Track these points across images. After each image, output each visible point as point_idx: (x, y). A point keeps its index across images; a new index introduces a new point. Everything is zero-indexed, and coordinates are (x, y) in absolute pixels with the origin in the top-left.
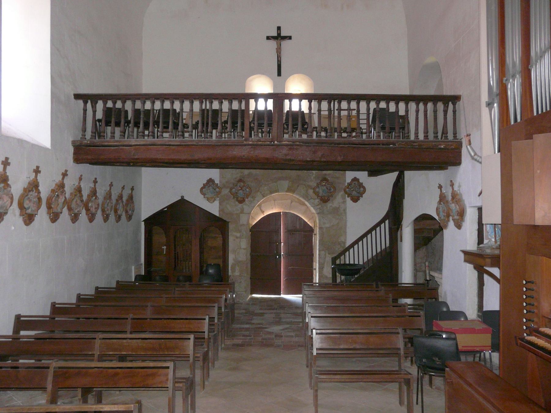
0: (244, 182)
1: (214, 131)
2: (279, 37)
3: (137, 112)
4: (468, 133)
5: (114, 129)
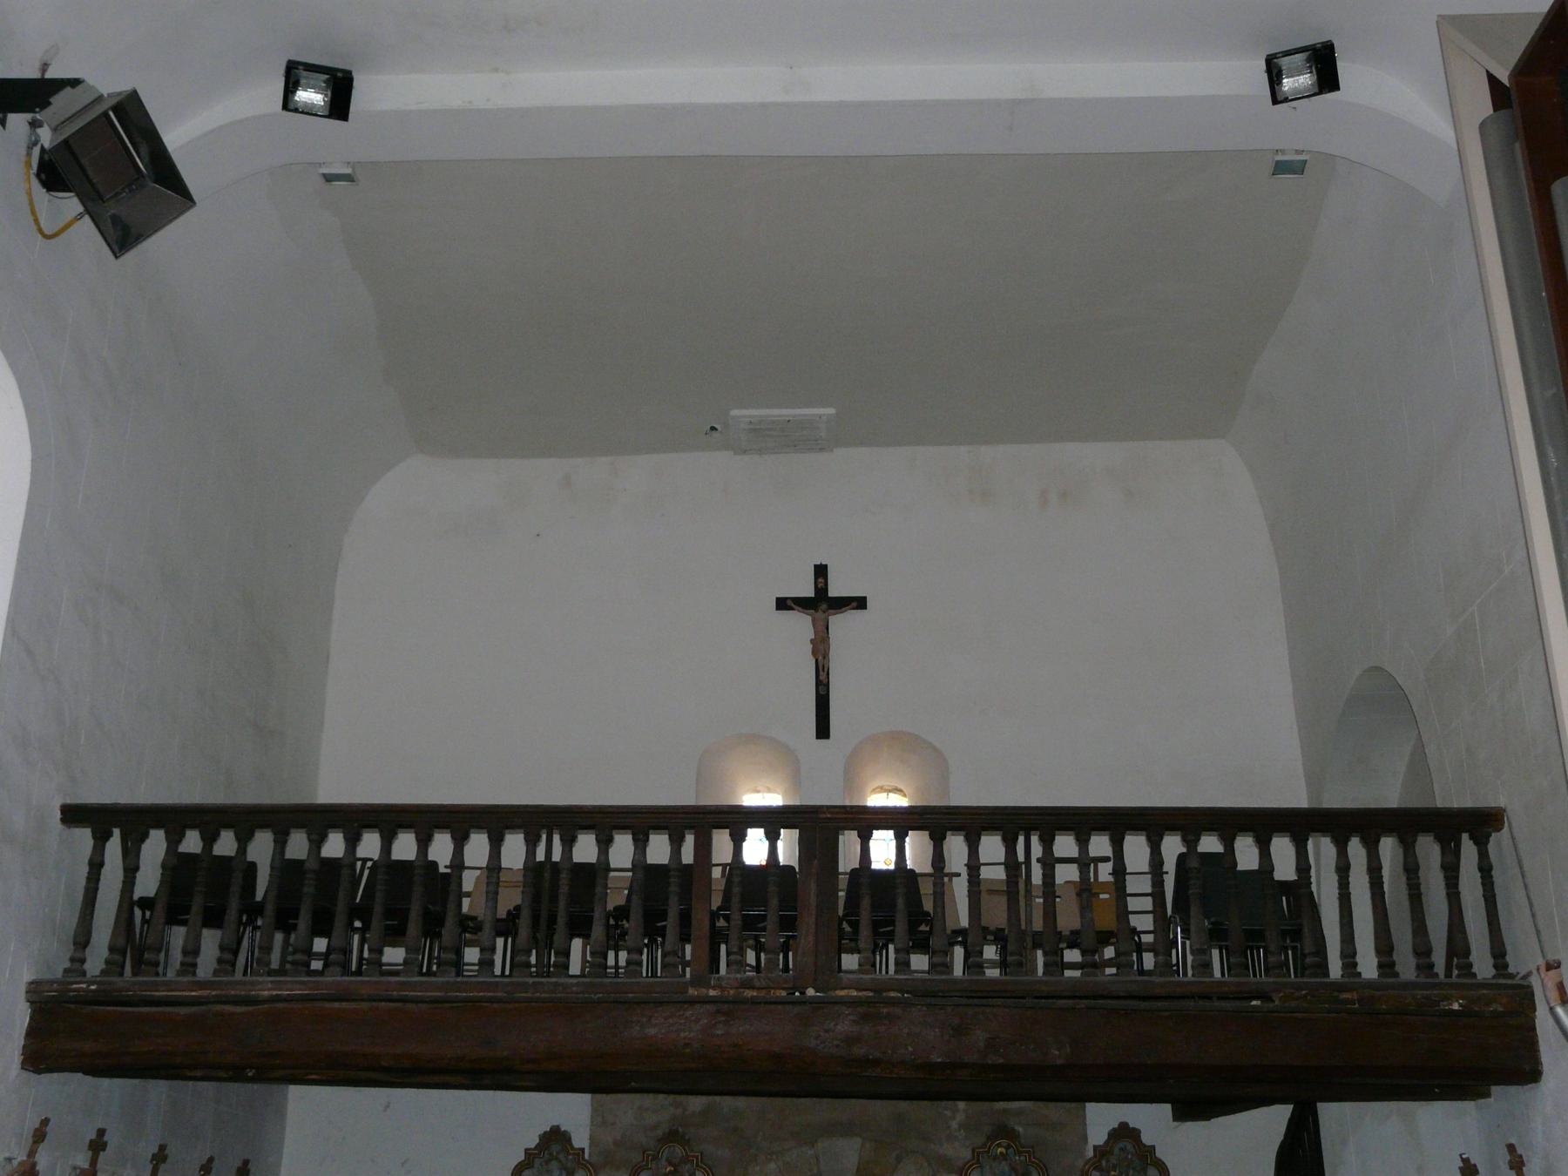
0: (685, 1142)
1: (577, 944)
2: (821, 603)
3: (288, 871)
4: (1551, 957)
5: (198, 937)
